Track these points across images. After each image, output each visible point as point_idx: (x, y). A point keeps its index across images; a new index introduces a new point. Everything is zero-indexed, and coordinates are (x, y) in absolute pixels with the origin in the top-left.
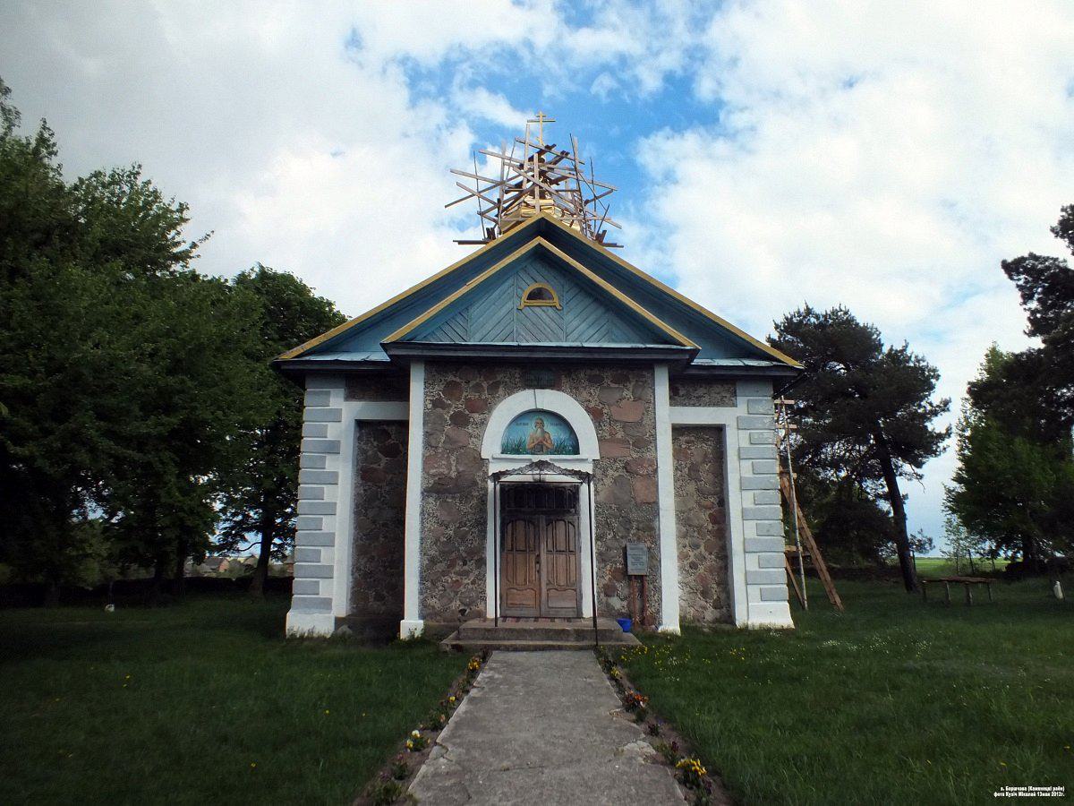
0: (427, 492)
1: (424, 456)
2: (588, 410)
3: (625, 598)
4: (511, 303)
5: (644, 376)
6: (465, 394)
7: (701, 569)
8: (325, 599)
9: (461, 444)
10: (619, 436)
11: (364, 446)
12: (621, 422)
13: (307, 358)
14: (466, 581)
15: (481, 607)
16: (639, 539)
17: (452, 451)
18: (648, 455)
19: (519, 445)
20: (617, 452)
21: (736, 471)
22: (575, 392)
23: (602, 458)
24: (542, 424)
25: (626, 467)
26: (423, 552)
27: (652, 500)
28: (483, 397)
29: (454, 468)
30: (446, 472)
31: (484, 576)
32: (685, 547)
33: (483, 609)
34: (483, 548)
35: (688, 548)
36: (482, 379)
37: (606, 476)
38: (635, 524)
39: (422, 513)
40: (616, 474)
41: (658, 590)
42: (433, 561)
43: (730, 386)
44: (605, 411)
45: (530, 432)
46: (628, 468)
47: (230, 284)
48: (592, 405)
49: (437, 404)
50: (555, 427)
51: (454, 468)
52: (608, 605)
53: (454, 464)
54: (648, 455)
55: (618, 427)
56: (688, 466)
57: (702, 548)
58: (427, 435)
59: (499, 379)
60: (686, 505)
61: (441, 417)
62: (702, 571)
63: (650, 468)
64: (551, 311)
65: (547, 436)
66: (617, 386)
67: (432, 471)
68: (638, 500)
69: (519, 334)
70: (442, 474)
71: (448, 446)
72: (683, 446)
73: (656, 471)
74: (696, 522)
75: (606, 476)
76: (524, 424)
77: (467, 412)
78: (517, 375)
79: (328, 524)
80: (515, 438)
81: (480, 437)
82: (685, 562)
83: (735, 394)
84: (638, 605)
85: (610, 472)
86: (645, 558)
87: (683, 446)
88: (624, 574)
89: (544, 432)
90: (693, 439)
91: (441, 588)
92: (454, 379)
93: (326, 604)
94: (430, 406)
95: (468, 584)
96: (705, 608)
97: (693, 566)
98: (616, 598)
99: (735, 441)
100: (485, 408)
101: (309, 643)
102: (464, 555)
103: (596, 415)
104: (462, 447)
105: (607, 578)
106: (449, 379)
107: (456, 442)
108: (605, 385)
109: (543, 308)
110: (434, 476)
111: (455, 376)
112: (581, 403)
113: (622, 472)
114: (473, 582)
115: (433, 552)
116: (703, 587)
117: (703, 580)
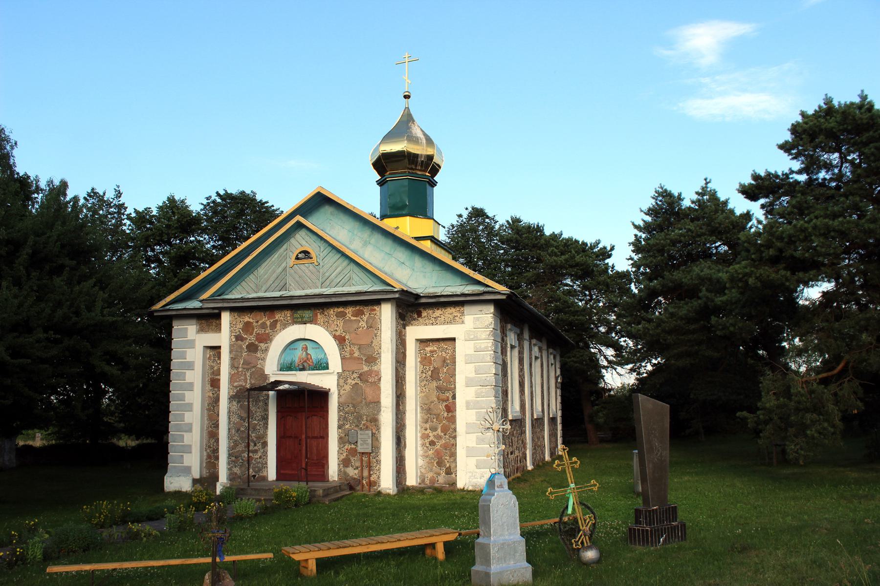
0: (231, 398)
1: (230, 373)
2: (335, 337)
3: (357, 468)
4: (285, 263)
5: (375, 310)
6: (255, 330)
7: (438, 446)
8: (187, 466)
9: (253, 365)
10: (356, 355)
11: (212, 364)
12: (357, 345)
13: (168, 307)
14: (256, 457)
15: (265, 474)
16: (367, 427)
17: (248, 369)
18: (375, 368)
19: (291, 364)
20: (353, 366)
21: (464, 371)
22: (326, 326)
23: (344, 371)
24: (306, 348)
25: (360, 377)
26: (230, 437)
27: (376, 401)
28: (267, 332)
29: (248, 381)
30: (244, 384)
31: (266, 453)
32: (426, 430)
33: (266, 474)
34: (265, 435)
35: (429, 431)
36: (266, 319)
37: (346, 384)
38: (365, 417)
39: (229, 412)
40: (353, 382)
41: (379, 462)
42: (236, 444)
43: (460, 307)
44: (347, 337)
45: (297, 355)
46: (362, 378)
47: (155, 213)
48: (338, 333)
49: (239, 338)
50: (440, 272)
51: (248, 381)
52: (345, 473)
53: (248, 378)
54: (375, 368)
55: (355, 349)
56: (432, 369)
57: (439, 430)
58: (232, 359)
59: (277, 318)
60: (428, 399)
61: (241, 347)
62: (438, 447)
63: (376, 377)
64: (311, 267)
65: (309, 357)
66: (356, 318)
67: (236, 384)
68: (368, 401)
69: (290, 285)
70: (242, 386)
71: (245, 367)
72: (428, 355)
73: (380, 379)
74: (435, 411)
75: (346, 384)
76: (295, 349)
77: (257, 343)
78: (288, 315)
79: (188, 417)
80: (288, 359)
81: (264, 359)
82: (426, 441)
83: (463, 314)
84: (366, 474)
85: (349, 381)
86: (370, 441)
87: (428, 355)
88: (353, 452)
89: (307, 354)
90: (435, 348)
91: (241, 461)
92: (249, 320)
93: (187, 470)
94: (234, 340)
95: (257, 458)
96: (439, 474)
97: (432, 443)
98: (351, 468)
99: (462, 349)
100: (266, 339)
101: (178, 495)
102: (255, 439)
103: (340, 340)
104: (253, 367)
105: (345, 454)
106: (246, 321)
107: (250, 363)
108: (348, 318)
109: (306, 265)
110: (236, 387)
111: (250, 318)
112: (331, 333)
113: (357, 381)
114: (260, 457)
115: (235, 438)
116: (438, 458)
117: (437, 453)
